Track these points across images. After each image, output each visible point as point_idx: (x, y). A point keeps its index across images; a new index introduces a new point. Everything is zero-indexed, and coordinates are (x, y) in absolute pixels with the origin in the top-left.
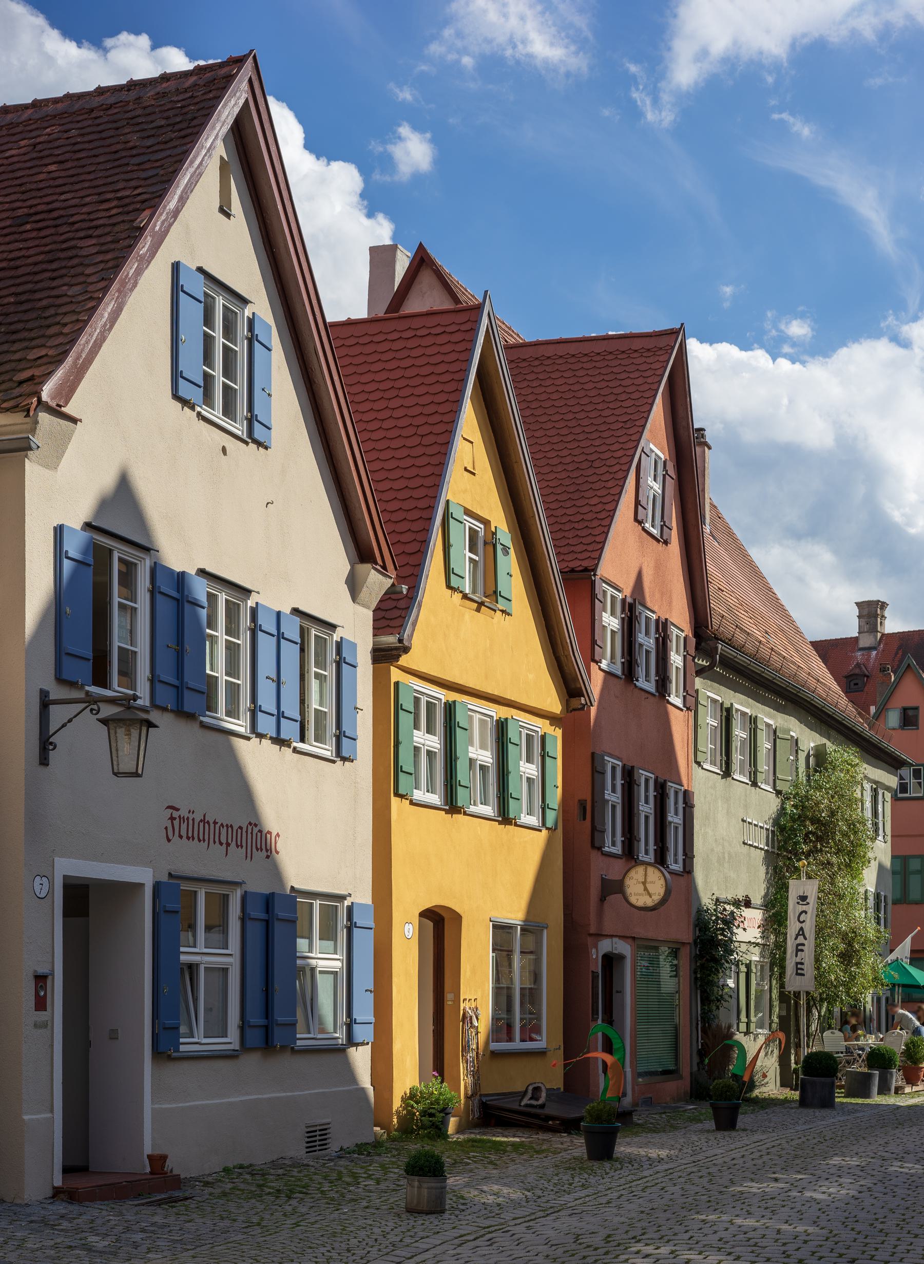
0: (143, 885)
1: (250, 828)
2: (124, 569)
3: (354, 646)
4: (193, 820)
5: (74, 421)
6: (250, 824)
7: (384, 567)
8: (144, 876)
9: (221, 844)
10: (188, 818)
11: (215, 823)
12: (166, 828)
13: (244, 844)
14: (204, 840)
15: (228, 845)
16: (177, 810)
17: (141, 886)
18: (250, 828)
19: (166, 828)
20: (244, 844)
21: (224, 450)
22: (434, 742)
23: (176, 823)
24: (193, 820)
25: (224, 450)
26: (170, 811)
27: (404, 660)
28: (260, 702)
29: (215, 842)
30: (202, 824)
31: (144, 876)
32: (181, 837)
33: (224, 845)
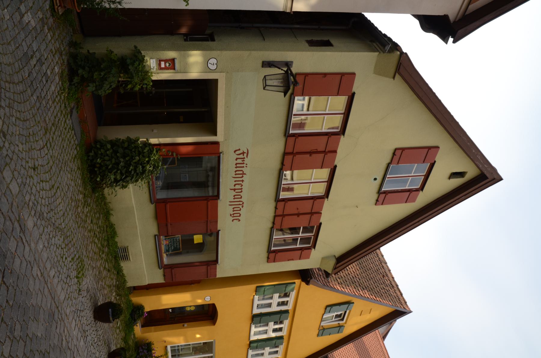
0: (216, 135)
1: (241, 203)
2: (285, 303)
3: (308, 257)
4: (243, 167)
5: (394, 78)
6: (243, 203)
7: (335, 269)
8: (219, 138)
9: (235, 185)
10: (244, 163)
11: (243, 181)
12: (239, 150)
13: (236, 200)
14: (236, 174)
15: (235, 190)
16: (247, 157)
17: (215, 134)
18: (241, 203)
19: (239, 150)
20: (236, 200)
21: (375, 179)
22: (275, 308)
23: (241, 156)
24: (243, 167)
25: (375, 179)
26: (246, 151)
27: (303, 284)
28: (297, 156)
29: (235, 181)
30: (241, 172)
31: (219, 138)
32: (236, 159)
33: (234, 188)
